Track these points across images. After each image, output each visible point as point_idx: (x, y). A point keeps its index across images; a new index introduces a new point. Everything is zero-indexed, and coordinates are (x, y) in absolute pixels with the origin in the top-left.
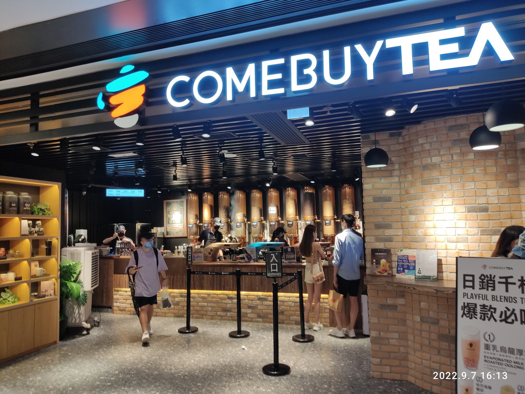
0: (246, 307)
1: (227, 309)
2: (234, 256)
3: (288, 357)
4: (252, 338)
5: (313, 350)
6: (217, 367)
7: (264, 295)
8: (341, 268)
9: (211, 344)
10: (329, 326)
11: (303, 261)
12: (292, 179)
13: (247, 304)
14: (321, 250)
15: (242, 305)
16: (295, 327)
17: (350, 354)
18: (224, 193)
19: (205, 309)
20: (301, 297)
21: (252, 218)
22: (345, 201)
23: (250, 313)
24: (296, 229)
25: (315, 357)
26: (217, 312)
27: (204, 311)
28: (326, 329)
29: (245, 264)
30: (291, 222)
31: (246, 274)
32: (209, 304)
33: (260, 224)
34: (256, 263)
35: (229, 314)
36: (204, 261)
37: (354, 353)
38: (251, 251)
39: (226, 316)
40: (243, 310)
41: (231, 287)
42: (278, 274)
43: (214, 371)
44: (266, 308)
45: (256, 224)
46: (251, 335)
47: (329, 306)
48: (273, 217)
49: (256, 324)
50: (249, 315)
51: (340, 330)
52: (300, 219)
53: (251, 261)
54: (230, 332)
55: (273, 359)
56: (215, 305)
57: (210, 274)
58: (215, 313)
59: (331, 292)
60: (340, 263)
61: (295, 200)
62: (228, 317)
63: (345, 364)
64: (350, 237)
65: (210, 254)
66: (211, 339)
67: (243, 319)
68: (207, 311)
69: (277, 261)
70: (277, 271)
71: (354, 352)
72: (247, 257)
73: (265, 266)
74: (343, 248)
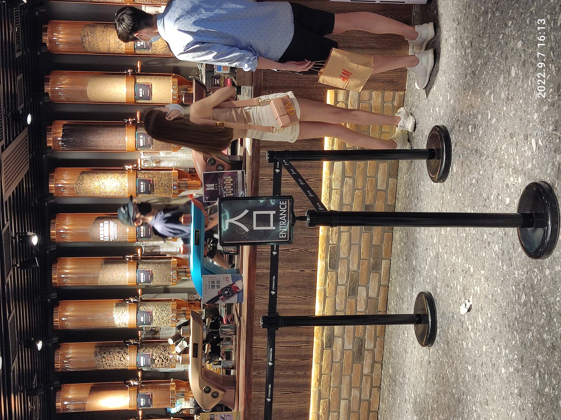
0: (351, 300)
1: (356, 349)
2: (225, 330)
3: (495, 192)
4: (435, 289)
5: (475, 127)
6: (526, 383)
7: (324, 255)
8: (263, 51)
9: (453, 395)
10: (402, 93)
11: (240, 152)
12: (22, 176)
13: (346, 298)
14: (215, 97)
15: (348, 313)
16: (403, 176)
17: (485, 29)
18: (58, 358)
19: (354, 407)
20: (333, 156)
21: (127, 284)
22: (87, 45)
23: (367, 290)
24: (158, 174)
25: (494, 120)
26: (362, 375)
27: (359, 409)
28: (409, 99)
29: (245, 304)
30: (140, 185)
31: (273, 300)
32: (344, 395)
33: (145, 263)
34: (245, 274)
35: (369, 345)
36: (235, 410)
38: (213, 287)
39: (372, 351)
40: (361, 310)
41: (304, 338)
42: (284, 210)
43: (539, 392)
44: (355, 248)
45: (142, 274)
46: (428, 289)
47: (357, 86)
48: (128, 230)
49: (393, 275)
50: (372, 294)
51: (416, 61)
52: (132, 162)
53: (238, 288)
55: (499, 231)
56: (346, 380)
57: (271, 398)
58: (364, 378)
59: (323, 81)
60: (250, 51)
61: (83, 173)
62: (375, 346)
63: (519, 38)
64: (178, 19)
65: (218, 394)
66: (438, 394)
67: (380, 311)
68: (360, 400)
69: (246, 211)
70: (274, 212)
71: (478, 20)
72: (228, 296)
73: (254, 246)
74: (210, 40)
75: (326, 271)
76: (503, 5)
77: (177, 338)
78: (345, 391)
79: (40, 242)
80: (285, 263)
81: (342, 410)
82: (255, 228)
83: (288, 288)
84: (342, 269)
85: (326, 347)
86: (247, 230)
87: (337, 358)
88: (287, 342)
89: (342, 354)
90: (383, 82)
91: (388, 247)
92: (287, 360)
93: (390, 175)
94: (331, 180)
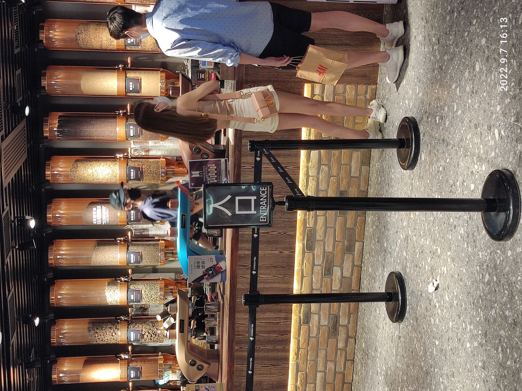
0: (327, 279)
1: (331, 325)
2: (210, 307)
3: (460, 179)
4: (404, 269)
5: (442, 118)
6: (489, 356)
7: (301, 237)
8: (244, 48)
9: (422, 368)
10: (374, 87)
12: (20, 164)
13: (322, 277)
14: (200, 90)
15: (324, 291)
16: (375, 164)
18: (54, 333)
19: (330, 379)
20: (310, 145)
21: (118, 264)
22: (81, 42)
23: (342, 270)
24: (147, 162)
25: (460, 112)
26: (337, 349)
27: (334, 380)
28: (381, 92)
29: (228, 283)
30: (130, 172)
31: (254, 279)
32: (320, 367)
33: (135, 245)
34: (228, 255)
35: (343, 321)
36: (219, 382)
37: (448, 18)
38: (198, 267)
39: (346, 326)
40: (336, 288)
41: (283, 315)
42: (264, 195)
43: (502, 365)
44: (330, 231)
45: (132, 255)
46: (398, 269)
47: (332, 80)
49: (366, 256)
50: (346, 274)
51: (387, 57)
52: (123, 151)
53: (221, 268)
54: (388, 319)
55: (464, 215)
56: (322, 354)
58: (339, 352)
59: (301, 75)
60: (233, 47)
61: (77, 161)
62: (349, 322)
63: (483, 35)
64: (166, 18)
65: (203, 367)
66: (408, 366)
67: (354, 289)
68: (335, 372)
69: (229, 197)
70: (255, 198)
71: (445, 18)
72: (212, 276)
73: (236, 229)
74: (196, 37)
75: (304, 253)
76: (468, 5)
77: (165, 315)
78: (321, 364)
79: (37, 225)
80: (265, 245)
81: (318, 382)
82: (237, 212)
83: (268, 268)
84: (318, 251)
85: (303, 323)
86: (230, 214)
87: (314, 333)
88: (267, 319)
89: (319, 329)
90: (356, 77)
91: (361, 229)
92: (267, 335)
93: (363, 163)
94: (308, 167)
